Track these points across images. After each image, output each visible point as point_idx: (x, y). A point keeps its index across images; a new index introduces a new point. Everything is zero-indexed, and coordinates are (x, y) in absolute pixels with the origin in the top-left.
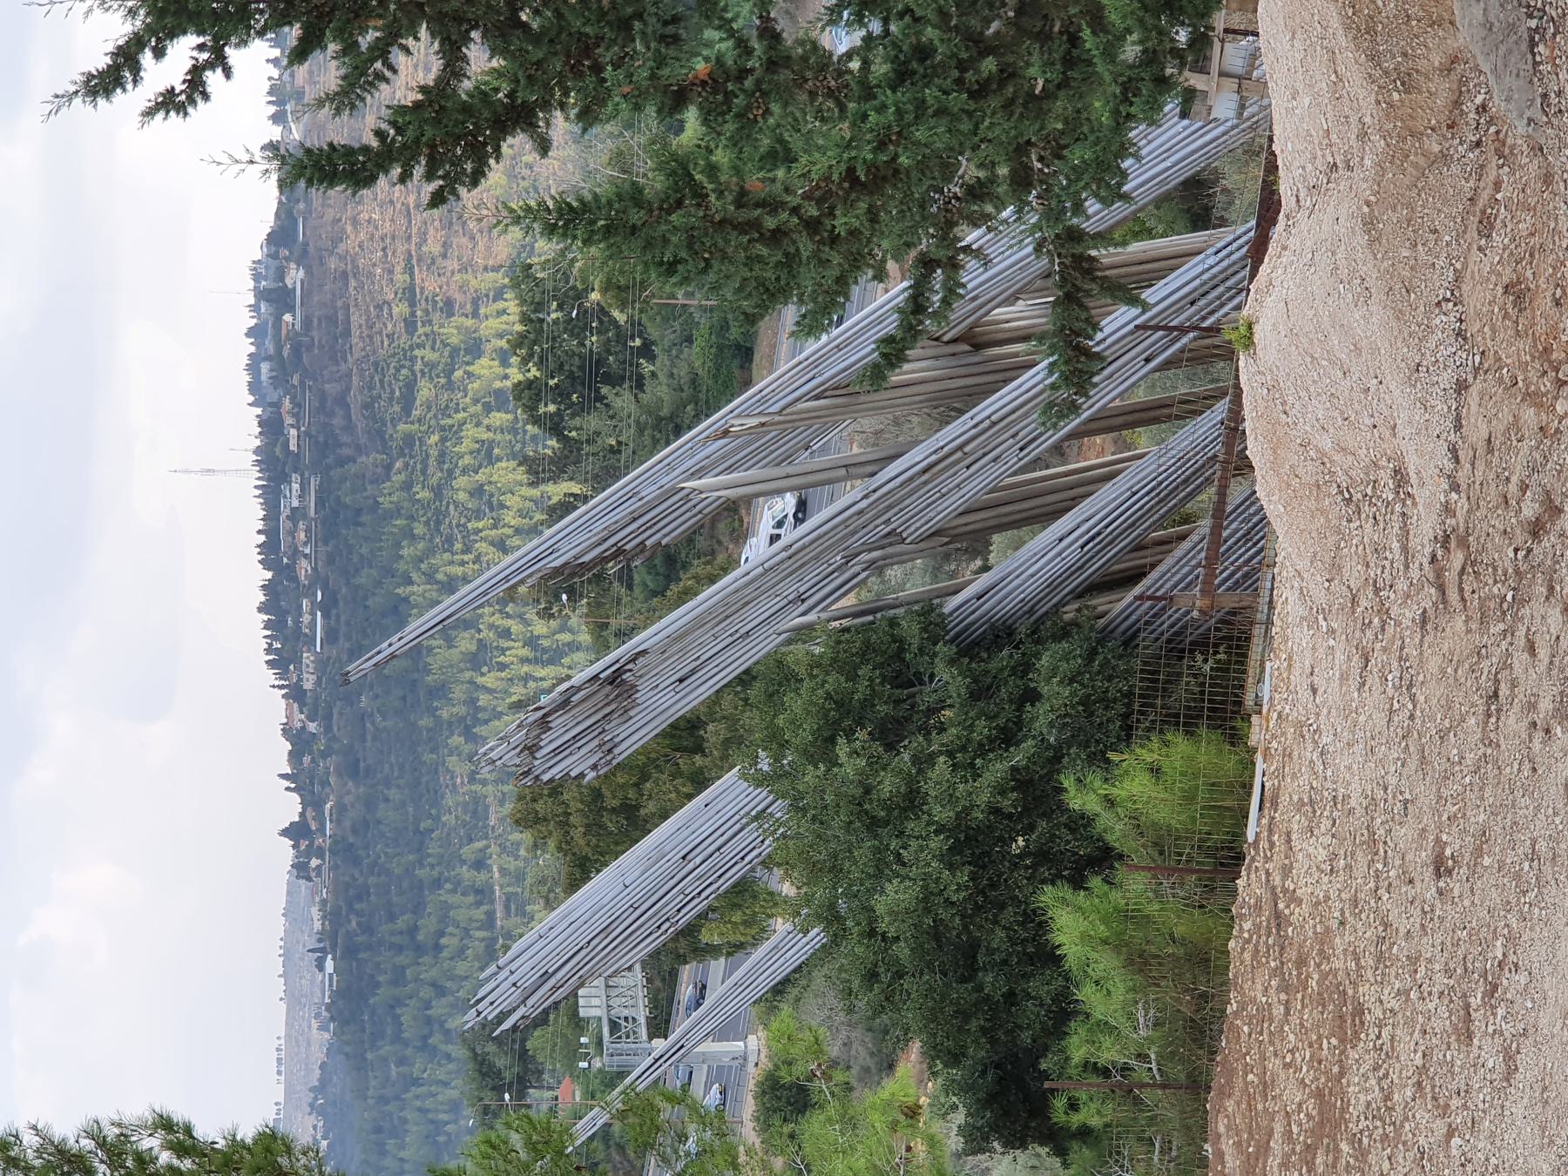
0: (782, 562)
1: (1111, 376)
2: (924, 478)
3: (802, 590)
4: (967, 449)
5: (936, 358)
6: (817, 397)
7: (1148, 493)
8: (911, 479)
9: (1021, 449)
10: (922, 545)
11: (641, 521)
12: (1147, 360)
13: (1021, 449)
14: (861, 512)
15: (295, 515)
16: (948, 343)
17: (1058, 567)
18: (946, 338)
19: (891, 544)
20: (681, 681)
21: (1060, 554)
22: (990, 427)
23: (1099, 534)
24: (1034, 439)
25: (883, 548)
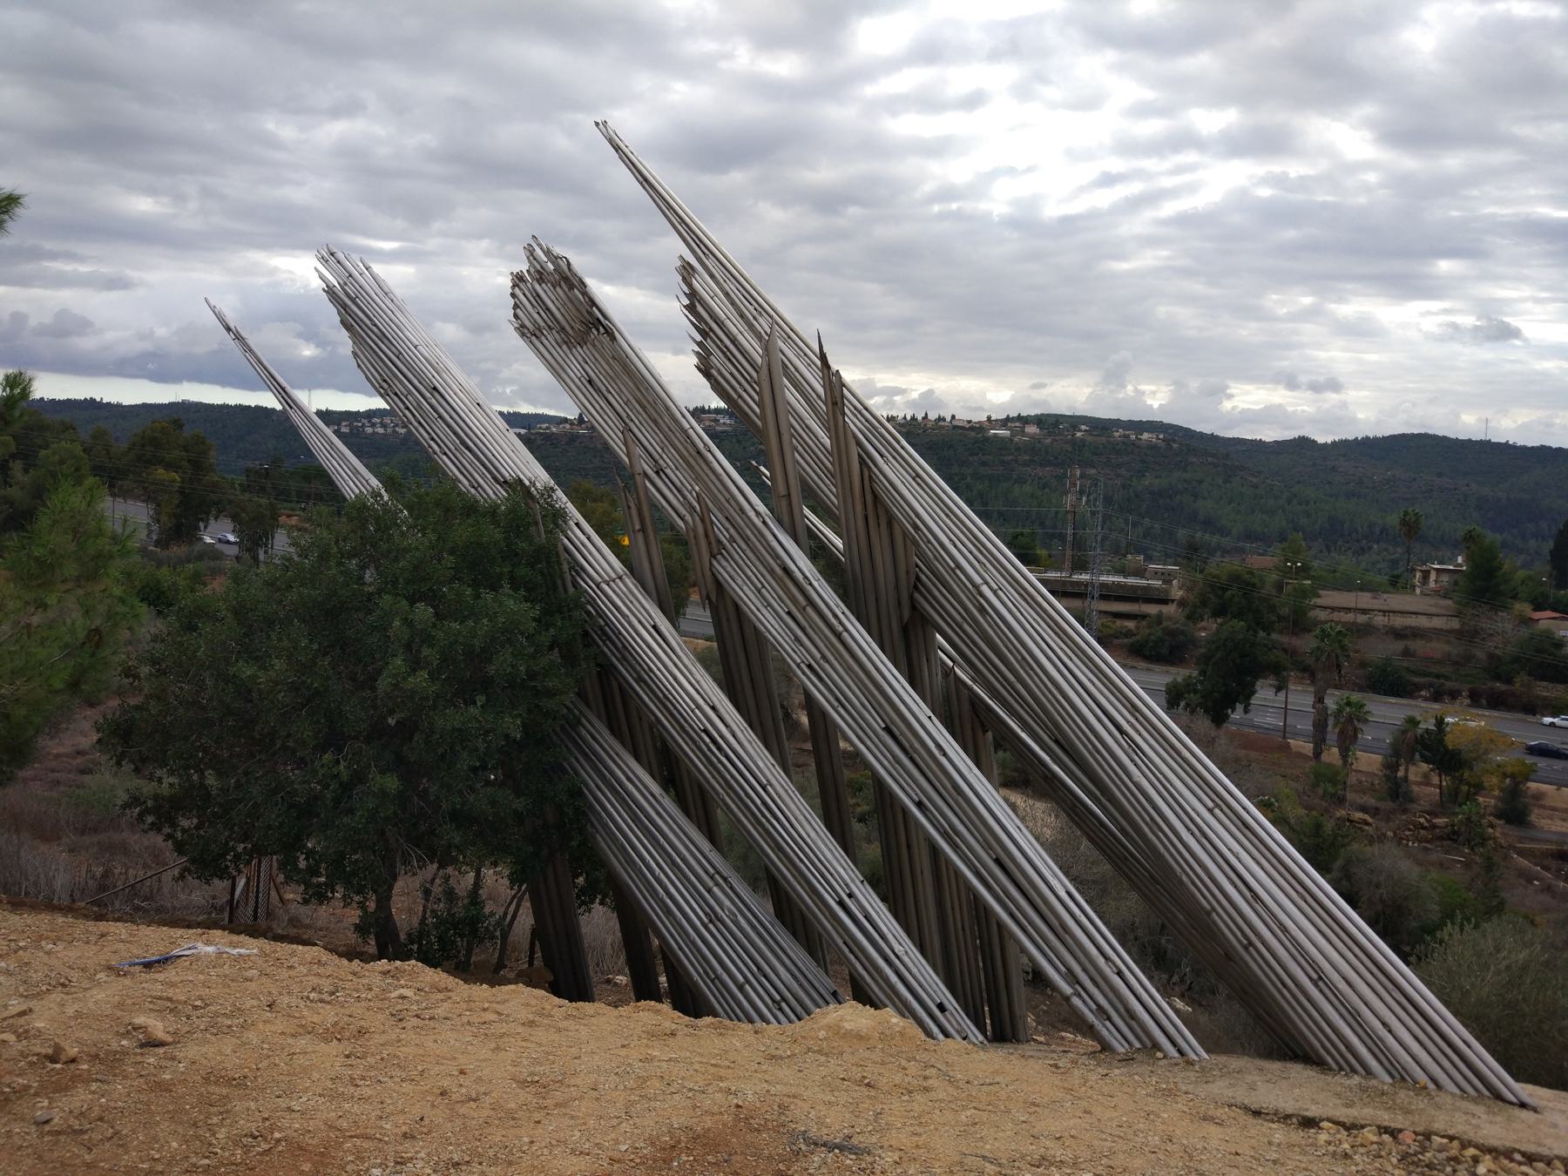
0: (694, 445)
1: (899, 762)
2: (778, 570)
3: (668, 471)
4: (809, 609)
5: (897, 587)
6: (862, 462)
7: (764, 803)
8: (776, 557)
9: (810, 666)
10: (708, 574)
11: (732, 347)
12: (919, 805)
13: (810, 666)
14: (742, 511)
15: (716, 421)
16: (911, 597)
17: (684, 704)
18: (917, 595)
19: (709, 544)
20: (590, 382)
21: (698, 707)
22: (974, 584)
23: (720, 748)
24: (821, 679)
25: (707, 536)
